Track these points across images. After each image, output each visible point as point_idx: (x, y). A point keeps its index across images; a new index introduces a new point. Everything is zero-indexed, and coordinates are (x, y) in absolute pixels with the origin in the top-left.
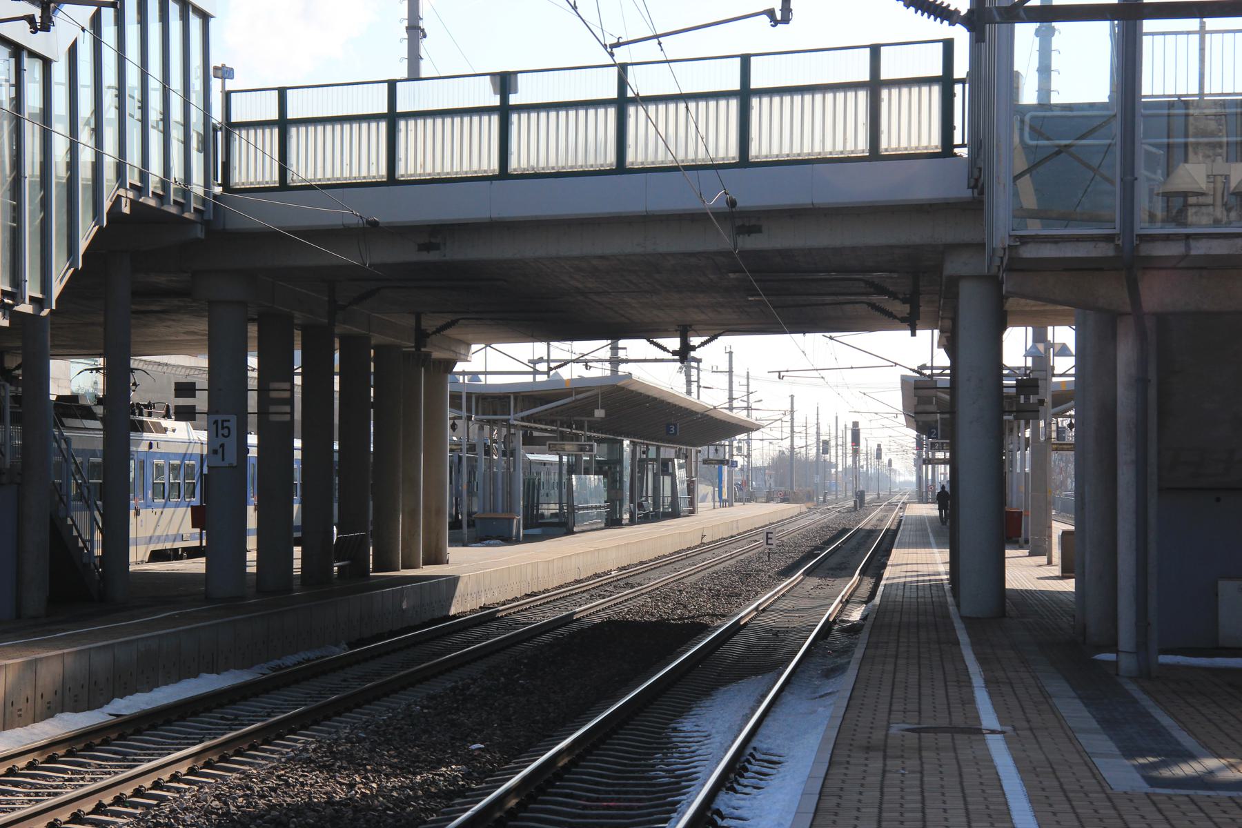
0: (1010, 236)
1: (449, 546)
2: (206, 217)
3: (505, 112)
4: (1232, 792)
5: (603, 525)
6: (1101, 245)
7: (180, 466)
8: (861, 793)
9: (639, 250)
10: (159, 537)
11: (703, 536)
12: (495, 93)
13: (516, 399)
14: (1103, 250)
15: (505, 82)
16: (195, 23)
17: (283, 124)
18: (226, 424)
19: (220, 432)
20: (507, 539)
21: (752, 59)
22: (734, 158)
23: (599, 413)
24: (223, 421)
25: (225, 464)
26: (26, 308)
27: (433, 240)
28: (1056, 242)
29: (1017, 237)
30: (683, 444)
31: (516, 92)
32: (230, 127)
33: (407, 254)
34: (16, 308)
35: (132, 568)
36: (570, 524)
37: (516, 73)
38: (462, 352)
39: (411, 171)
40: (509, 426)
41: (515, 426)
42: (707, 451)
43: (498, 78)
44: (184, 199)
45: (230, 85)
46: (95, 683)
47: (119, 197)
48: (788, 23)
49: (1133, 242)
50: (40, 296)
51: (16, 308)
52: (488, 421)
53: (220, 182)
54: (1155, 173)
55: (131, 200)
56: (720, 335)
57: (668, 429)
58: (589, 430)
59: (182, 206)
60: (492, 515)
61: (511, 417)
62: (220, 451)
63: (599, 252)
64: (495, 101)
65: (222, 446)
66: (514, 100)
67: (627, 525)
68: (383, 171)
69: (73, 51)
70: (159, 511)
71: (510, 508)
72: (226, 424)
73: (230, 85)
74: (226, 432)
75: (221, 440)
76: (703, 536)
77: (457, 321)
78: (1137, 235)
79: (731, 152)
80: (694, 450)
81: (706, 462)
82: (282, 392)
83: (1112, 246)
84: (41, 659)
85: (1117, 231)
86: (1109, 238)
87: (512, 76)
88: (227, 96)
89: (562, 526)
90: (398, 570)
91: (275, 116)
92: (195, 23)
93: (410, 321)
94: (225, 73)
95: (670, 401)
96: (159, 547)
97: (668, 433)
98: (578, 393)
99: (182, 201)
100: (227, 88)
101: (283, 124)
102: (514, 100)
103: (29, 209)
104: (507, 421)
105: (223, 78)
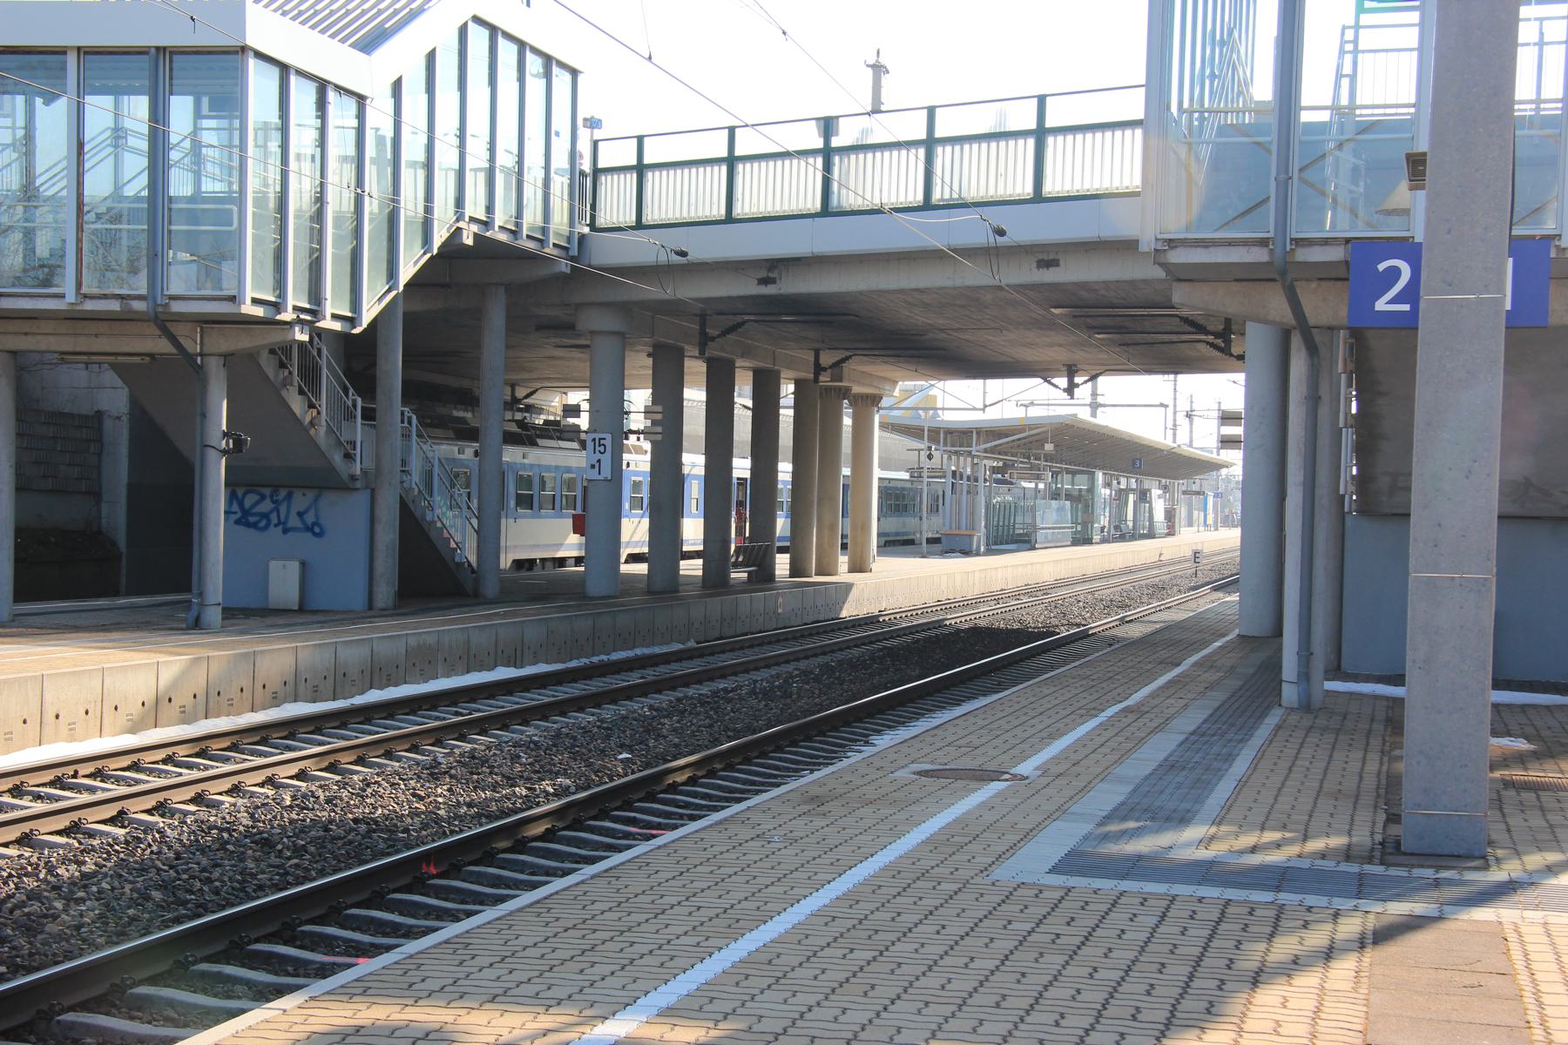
0: (1157, 239)
1: (880, 553)
2: (571, 253)
3: (827, 153)
5: (1069, 543)
6: (1255, 249)
8: (1268, 778)
9: (949, 283)
10: (637, 543)
11: (1160, 555)
12: (820, 136)
13: (978, 433)
14: (1258, 255)
15: (828, 126)
16: (561, 80)
17: (640, 169)
18: (602, 442)
19: (598, 448)
20: (966, 553)
21: (1048, 98)
22: (1028, 194)
23: (1049, 447)
24: (600, 439)
25: (601, 477)
26: (328, 324)
27: (771, 275)
28: (1207, 247)
29: (1165, 240)
30: (1169, 478)
31: (837, 135)
32: (597, 172)
33: (747, 287)
34: (317, 324)
35: (681, 572)
36: (1033, 541)
37: (837, 117)
38: (887, 388)
39: (747, 210)
40: (973, 457)
41: (978, 456)
42: (1181, 484)
43: (822, 122)
44: (544, 235)
45: (598, 134)
46: (344, 674)
47: (459, 229)
49: (1285, 247)
50: (350, 314)
51: (317, 324)
52: (956, 452)
53: (588, 222)
54: (1358, 186)
55: (475, 234)
56: (1100, 374)
57: (1134, 464)
58: (1046, 461)
59: (515, 233)
60: (957, 532)
61: (974, 449)
62: (597, 465)
63: (913, 285)
64: (819, 144)
65: (599, 461)
66: (836, 142)
67: (1096, 543)
68: (723, 211)
69: (397, 86)
70: (637, 520)
71: (973, 526)
72: (602, 442)
73: (598, 134)
74: (602, 449)
75: (598, 456)
76: (1160, 555)
77: (850, 357)
78: (1292, 240)
79: (1026, 188)
80: (1176, 482)
81: (1185, 493)
83: (1265, 250)
84: (262, 652)
85: (1271, 235)
86: (1263, 243)
87: (835, 120)
88: (595, 144)
89: (1025, 541)
90: (811, 577)
91: (634, 162)
92: (561, 80)
93: (811, 357)
94: (593, 123)
95: (156, 637)
96: (637, 551)
97: (1134, 467)
98: (1030, 429)
99: (540, 237)
100: (595, 138)
101: (640, 169)
102: (836, 142)
103: (333, 234)
104: (970, 452)
105: (592, 127)
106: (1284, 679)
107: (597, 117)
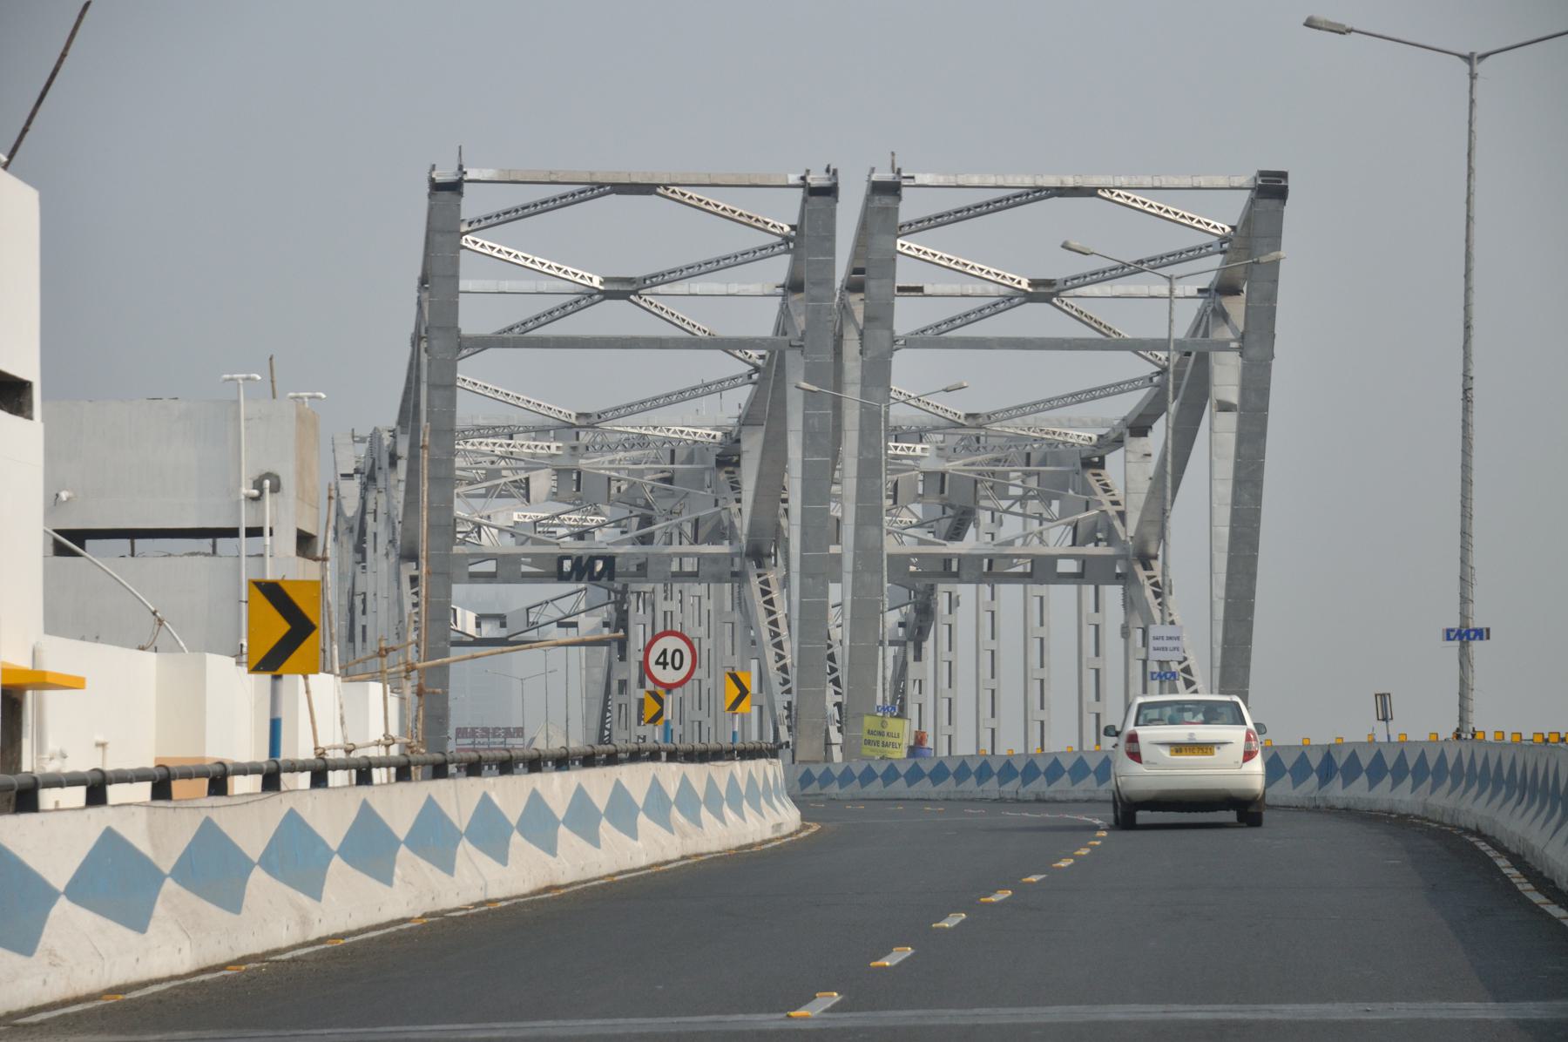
4: (130, 1040)
7: (430, 301)
48: (967, 414)
82: (389, 715)
106: (846, 429)
107: (1150, 434)
